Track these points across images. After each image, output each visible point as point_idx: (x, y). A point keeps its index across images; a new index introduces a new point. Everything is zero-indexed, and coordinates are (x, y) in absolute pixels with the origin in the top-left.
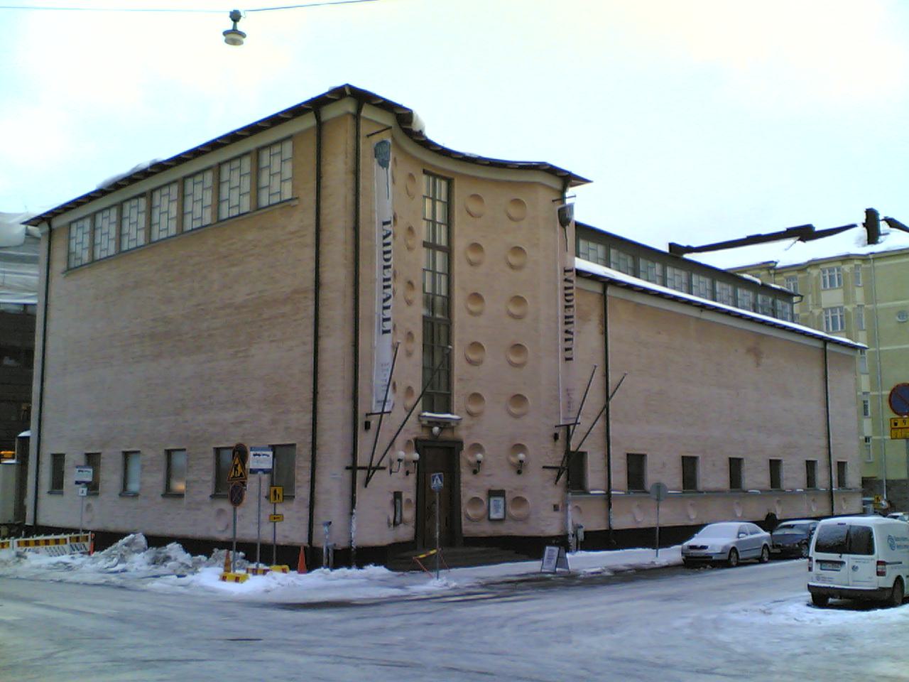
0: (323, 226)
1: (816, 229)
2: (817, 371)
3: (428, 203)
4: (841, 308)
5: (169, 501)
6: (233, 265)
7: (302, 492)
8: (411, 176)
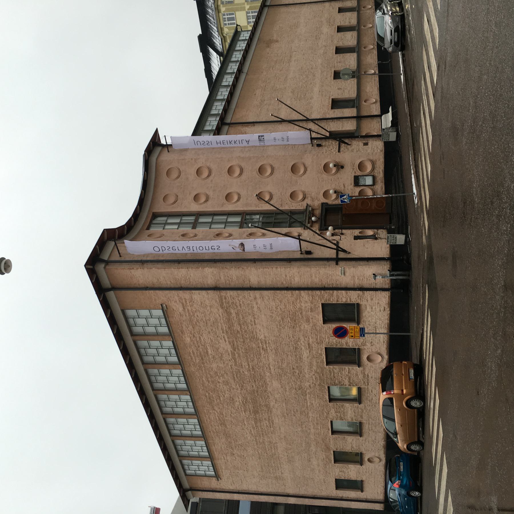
0: (178, 286)
1: (201, 33)
2: (283, 9)
3: (167, 227)
4: (247, 13)
5: (364, 398)
6: (207, 352)
7: (353, 297)
8: (149, 236)
